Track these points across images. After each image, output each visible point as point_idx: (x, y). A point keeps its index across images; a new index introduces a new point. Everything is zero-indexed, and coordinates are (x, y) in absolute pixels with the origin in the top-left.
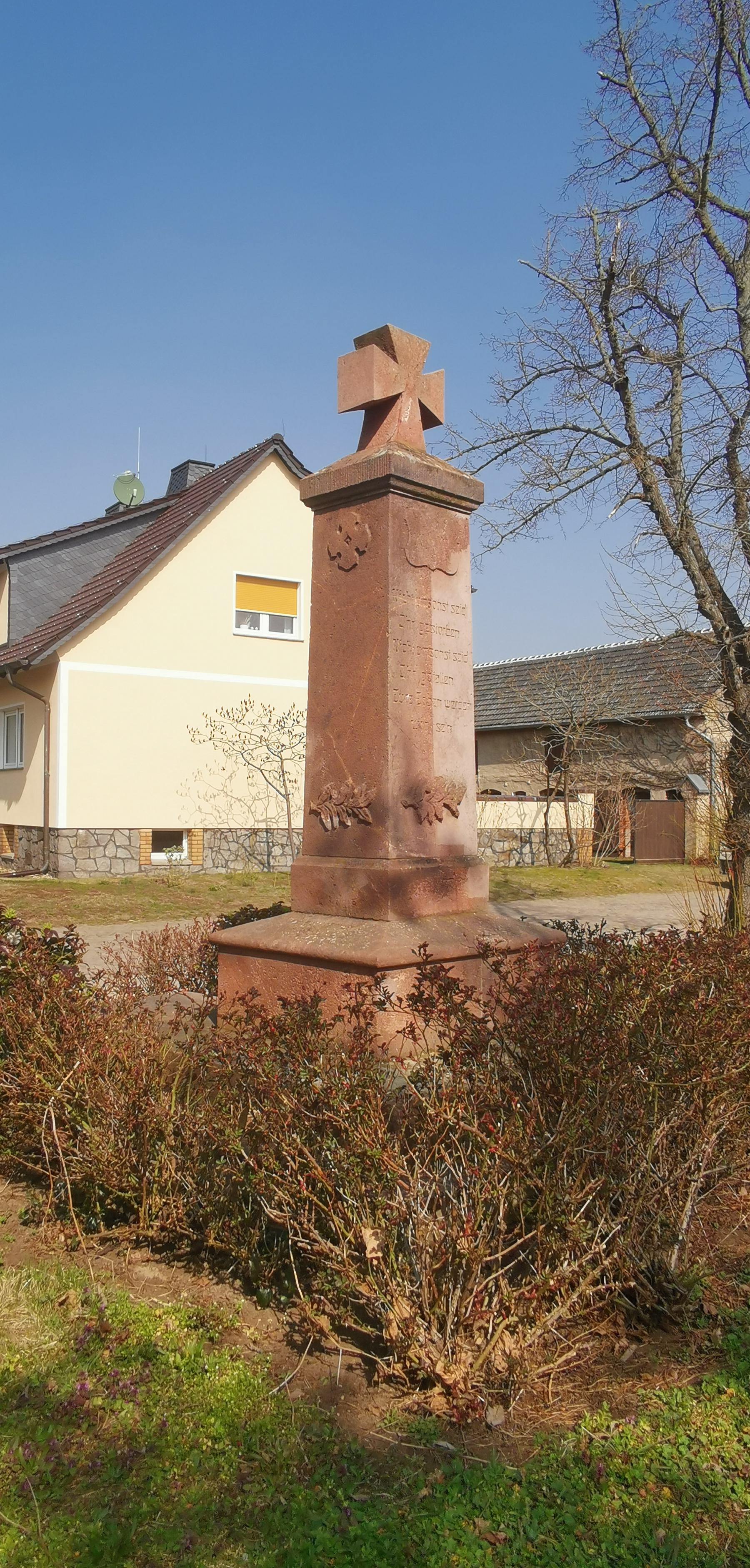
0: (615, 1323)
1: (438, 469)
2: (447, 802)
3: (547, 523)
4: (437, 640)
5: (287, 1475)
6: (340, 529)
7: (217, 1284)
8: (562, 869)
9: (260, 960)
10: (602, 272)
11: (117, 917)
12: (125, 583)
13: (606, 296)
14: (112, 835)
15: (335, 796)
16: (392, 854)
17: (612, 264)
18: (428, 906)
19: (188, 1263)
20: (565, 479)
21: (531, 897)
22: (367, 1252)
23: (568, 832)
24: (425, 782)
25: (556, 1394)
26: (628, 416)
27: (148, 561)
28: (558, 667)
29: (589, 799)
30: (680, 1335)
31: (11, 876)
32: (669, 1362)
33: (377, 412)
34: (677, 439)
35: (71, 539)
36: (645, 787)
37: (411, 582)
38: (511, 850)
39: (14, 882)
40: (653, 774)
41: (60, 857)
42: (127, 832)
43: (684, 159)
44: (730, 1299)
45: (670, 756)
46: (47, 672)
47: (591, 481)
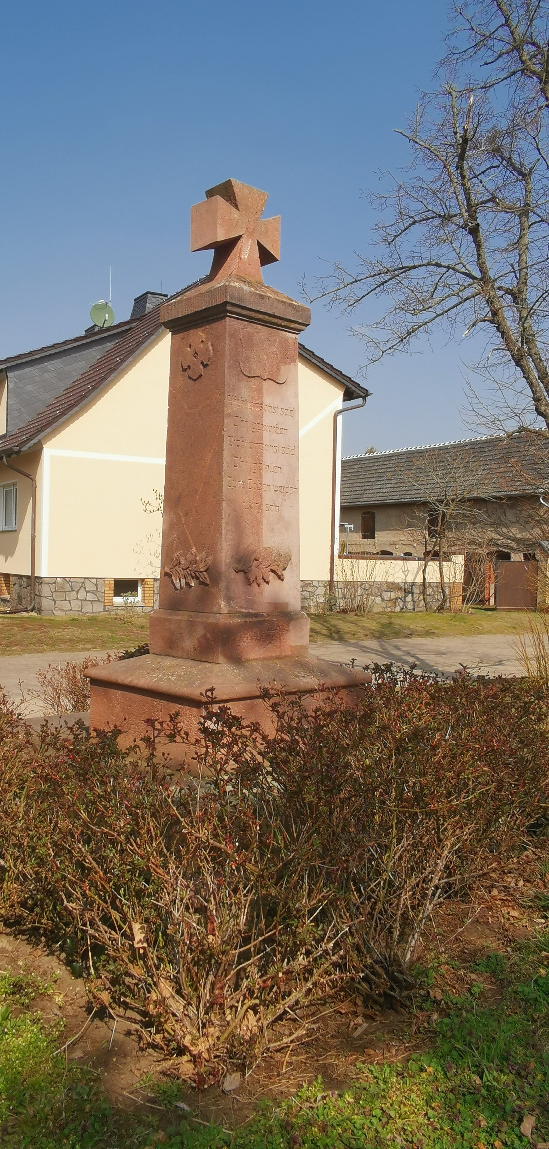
0: (355, 1004)
1: (269, 297)
2: (273, 568)
3: (416, 342)
4: (267, 437)
5: (43, 1128)
6: (190, 346)
7: (48, 955)
8: (437, 614)
9: (120, 692)
10: (458, 138)
11: (81, 646)
12: (94, 388)
13: (462, 157)
14: (83, 583)
15: (183, 562)
16: (222, 611)
17: (465, 131)
18: (252, 650)
19: (30, 937)
20: (426, 306)
21: (409, 636)
22: (135, 942)
23: (441, 585)
24: (254, 552)
25: (290, 1064)
26: (479, 255)
27: (112, 370)
28: (438, 456)
29: (460, 559)
30: (408, 1016)
31: (5, 613)
32: (392, 1039)
33: (223, 250)
34: (523, 274)
35: (56, 353)
36: (506, 551)
37: (245, 389)
38: (397, 599)
39: (5, 618)
40: (513, 540)
41: (43, 599)
42: (94, 581)
43: (534, 44)
44: (457, 986)
45: (527, 526)
46: (34, 456)
47: (453, 307)
